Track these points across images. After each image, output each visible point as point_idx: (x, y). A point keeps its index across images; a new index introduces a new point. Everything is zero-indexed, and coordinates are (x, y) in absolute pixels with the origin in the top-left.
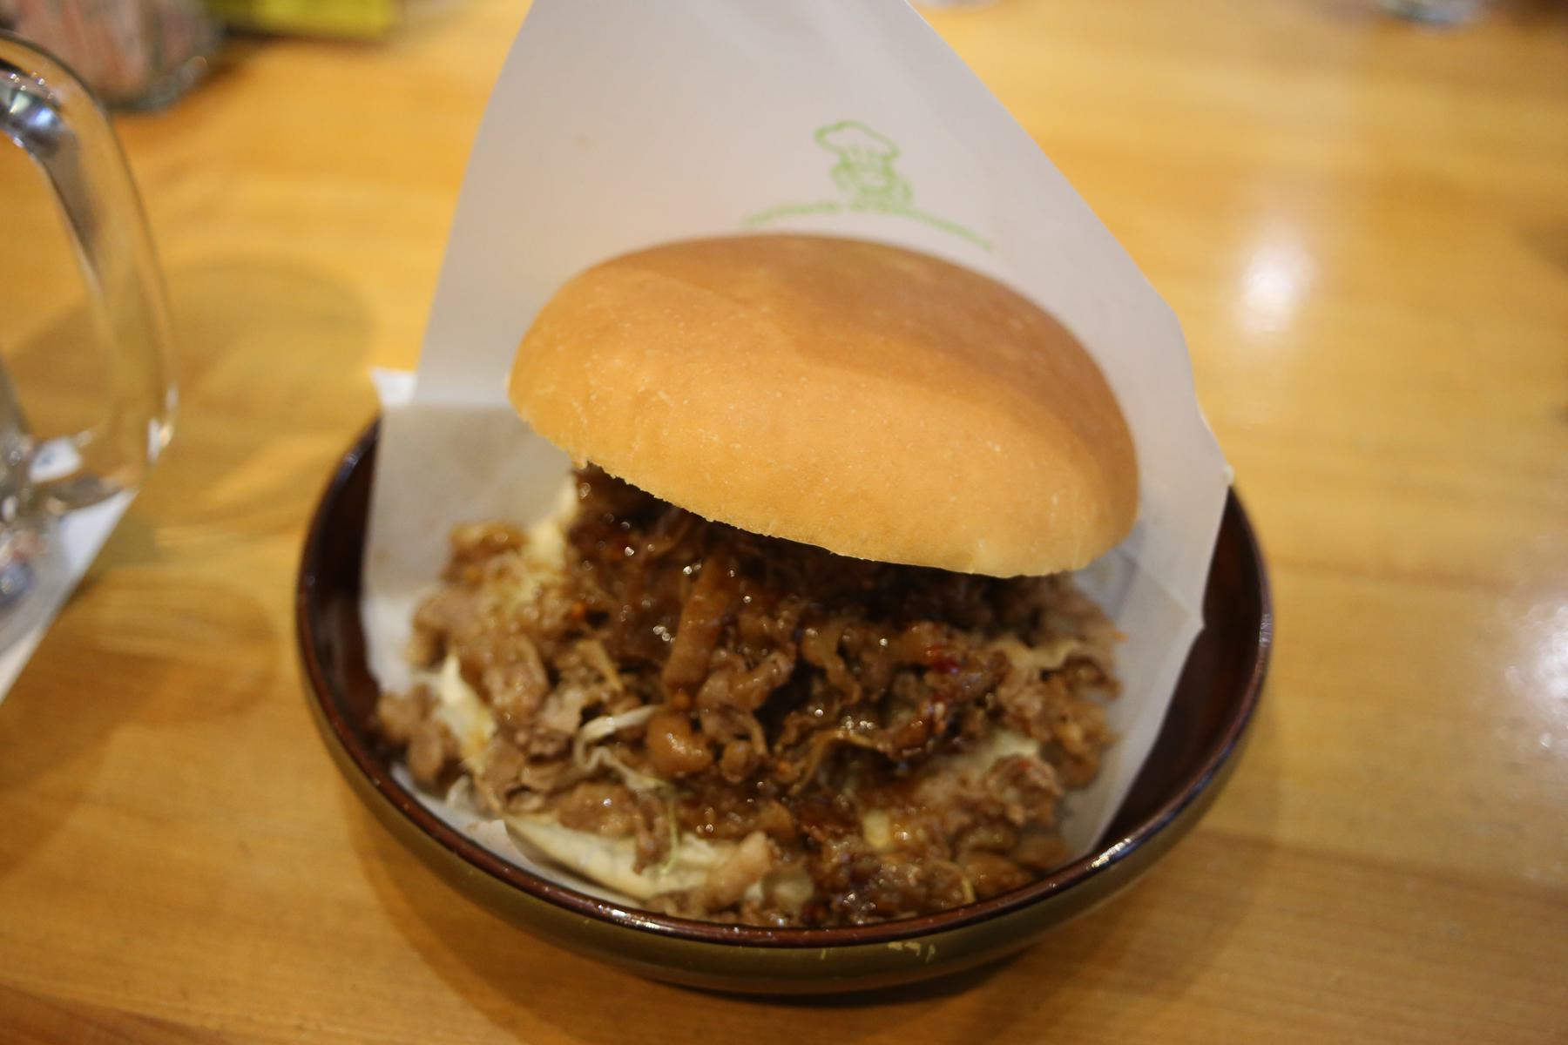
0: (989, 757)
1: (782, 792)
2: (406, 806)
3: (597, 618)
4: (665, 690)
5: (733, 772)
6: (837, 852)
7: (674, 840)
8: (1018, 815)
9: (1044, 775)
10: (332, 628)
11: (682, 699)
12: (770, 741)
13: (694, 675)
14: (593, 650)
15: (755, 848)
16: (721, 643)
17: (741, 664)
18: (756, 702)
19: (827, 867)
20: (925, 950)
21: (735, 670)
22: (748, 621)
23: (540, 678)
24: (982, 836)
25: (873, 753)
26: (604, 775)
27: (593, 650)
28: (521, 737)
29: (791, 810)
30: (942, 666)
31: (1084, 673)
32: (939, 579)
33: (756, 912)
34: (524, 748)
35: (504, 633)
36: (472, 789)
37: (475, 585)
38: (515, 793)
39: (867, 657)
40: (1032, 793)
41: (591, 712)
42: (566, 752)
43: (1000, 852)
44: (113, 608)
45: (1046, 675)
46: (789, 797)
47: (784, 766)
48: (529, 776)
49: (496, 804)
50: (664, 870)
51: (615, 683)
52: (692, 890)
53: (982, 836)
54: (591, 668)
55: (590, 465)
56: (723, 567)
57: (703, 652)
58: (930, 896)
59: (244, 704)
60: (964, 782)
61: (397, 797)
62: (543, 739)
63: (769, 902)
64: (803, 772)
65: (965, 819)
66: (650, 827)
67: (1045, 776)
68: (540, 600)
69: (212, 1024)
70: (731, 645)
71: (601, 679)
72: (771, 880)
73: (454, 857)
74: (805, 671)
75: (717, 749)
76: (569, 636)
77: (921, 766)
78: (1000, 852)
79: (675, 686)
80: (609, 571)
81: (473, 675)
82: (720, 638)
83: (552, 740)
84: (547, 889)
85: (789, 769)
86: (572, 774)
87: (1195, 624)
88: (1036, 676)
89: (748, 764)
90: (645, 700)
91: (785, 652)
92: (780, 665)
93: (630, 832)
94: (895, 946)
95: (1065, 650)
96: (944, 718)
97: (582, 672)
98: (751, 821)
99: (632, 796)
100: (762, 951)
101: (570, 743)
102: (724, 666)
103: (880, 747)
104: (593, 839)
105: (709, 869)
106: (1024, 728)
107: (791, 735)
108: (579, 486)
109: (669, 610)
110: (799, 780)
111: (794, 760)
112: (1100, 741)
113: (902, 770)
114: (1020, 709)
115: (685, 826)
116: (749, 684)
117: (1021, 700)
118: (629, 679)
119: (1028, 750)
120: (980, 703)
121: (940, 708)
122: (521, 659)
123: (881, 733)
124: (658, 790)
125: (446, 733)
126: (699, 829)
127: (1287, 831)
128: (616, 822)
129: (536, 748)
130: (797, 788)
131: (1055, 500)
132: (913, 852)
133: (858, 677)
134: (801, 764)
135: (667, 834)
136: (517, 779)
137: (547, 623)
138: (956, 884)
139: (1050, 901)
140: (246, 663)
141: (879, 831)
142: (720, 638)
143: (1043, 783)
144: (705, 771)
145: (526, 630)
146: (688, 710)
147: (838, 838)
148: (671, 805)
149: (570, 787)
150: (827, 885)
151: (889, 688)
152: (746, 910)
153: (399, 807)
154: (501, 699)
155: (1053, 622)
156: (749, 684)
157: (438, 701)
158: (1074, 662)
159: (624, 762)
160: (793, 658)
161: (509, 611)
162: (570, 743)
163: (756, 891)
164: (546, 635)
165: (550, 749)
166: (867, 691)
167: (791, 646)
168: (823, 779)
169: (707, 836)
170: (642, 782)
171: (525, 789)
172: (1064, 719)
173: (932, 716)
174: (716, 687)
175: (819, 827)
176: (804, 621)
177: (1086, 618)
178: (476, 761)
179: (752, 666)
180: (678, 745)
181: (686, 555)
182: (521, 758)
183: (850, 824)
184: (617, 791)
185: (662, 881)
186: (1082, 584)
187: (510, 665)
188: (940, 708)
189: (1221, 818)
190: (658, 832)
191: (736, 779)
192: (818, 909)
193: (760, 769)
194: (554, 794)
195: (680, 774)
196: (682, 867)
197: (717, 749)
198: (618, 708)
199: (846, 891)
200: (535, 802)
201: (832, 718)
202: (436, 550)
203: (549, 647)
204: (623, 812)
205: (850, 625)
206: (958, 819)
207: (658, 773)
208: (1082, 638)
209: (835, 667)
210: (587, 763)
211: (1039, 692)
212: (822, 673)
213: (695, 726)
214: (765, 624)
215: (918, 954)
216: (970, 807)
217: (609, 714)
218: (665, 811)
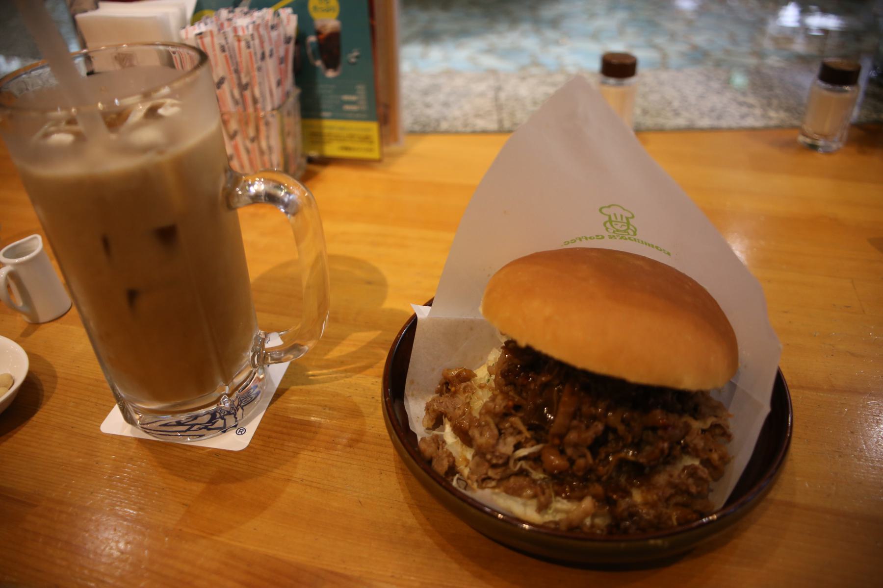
0: (680, 466)
1: (599, 480)
2: (444, 484)
3: (517, 408)
6: (623, 504)
7: (553, 499)
8: (693, 489)
9: (704, 472)
11: (557, 441)
14: (516, 420)
15: (587, 503)
17: (583, 426)
18: (589, 441)
19: (620, 510)
22: (585, 409)
23: (496, 432)
24: (679, 499)
26: (522, 473)
27: (516, 420)
30: (665, 427)
31: (718, 431)
40: (700, 480)
41: (518, 446)
42: (506, 464)
43: (684, 505)
44: (293, 402)
45: (704, 431)
48: (491, 473)
50: (550, 512)
51: (527, 434)
52: (561, 520)
53: (679, 499)
54: (515, 429)
60: (671, 476)
62: (497, 457)
65: (672, 491)
71: (520, 433)
73: (465, 505)
74: (609, 429)
75: (572, 462)
76: (505, 415)
77: (655, 470)
78: (684, 505)
80: (520, 389)
82: (574, 416)
83: (501, 458)
85: (602, 470)
86: (508, 472)
88: (700, 432)
90: (538, 442)
92: (600, 427)
93: (535, 496)
95: (710, 421)
97: (511, 430)
98: (586, 491)
99: (534, 481)
101: (508, 458)
104: (519, 499)
105: (567, 512)
106: (696, 453)
107: (603, 455)
112: (725, 460)
113: (647, 470)
115: (558, 494)
117: (696, 441)
118: (532, 433)
119: (697, 463)
120: (679, 443)
121: (666, 445)
124: (544, 478)
125: (450, 455)
126: (563, 495)
128: (529, 492)
129: (494, 461)
130: (605, 478)
132: (653, 505)
134: (606, 468)
135: (551, 497)
136: (486, 474)
138: (670, 518)
141: (637, 496)
143: (705, 476)
148: (551, 486)
149: (509, 477)
153: (440, 484)
157: (444, 442)
158: (715, 426)
159: (531, 467)
165: (501, 462)
168: (614, 474)
169: (568, 498)
170: (538, 475)
171: (489, 478)
172: (711, 450)
174: (572, 436)
176: (608, 409)
177: (717, 408)
179: (588, 427)
180: (555, 460)
183: (628, 494)
184: (528, 479)
185: (548, 517)
186: (713, 395)
189: (778, 494)
191: (580, 474)
192: (615, 528)
193: (590, 470)
194: (500, 481)
196: (557, 511)
197: (572, 462)
198: (528, 445)
199: (626, 520)
200: (493, 483)
202: (435, 379)
206: (669, 491)
208: (716, 416)
209: (621, 428)
212: (615, 431)
214: (593, 410)
217: (525, 447)
218: (549, 488)
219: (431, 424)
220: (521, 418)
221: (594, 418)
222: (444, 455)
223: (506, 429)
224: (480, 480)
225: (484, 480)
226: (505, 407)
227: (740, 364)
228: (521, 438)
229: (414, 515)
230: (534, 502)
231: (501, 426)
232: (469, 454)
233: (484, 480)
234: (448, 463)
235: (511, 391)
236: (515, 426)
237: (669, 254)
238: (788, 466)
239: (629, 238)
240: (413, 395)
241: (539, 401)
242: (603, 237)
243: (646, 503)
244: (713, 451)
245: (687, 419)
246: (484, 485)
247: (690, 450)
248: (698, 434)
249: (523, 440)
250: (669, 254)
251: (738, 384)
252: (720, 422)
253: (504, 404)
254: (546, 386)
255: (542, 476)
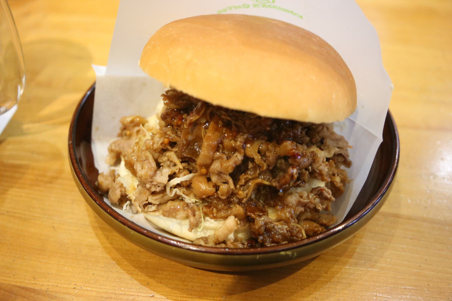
1: (240, 202)
3: (173, 144)
4: (198, 167)
5: (222, 195)
6: (260, 221)
10: (81, 153)
11: (204, 171)
12: (235, 184)
13: (208, 161)
14: (172, 155)
15: (231, 222)
16: (217, 150)
17: (225, 157)
18: (230, 171)
20: (293, 254)
21: (222, 159)
23: (154, 165)
25: (270, 187)
26: (177, 198)
27: (172, 155)
28: (148, 186)
29: (243, 208)
31: (340, 159)
32: (293, 124)
33: (232, 243)
34: (149, 189)
35: (139, 150)
36: (131, 205)
37: (130, 136)
38: (147, 204)
39: (268, 154)
41: (171, 177)
42: (164, 190)
45: (328, 159)
46: (242, 204)
47: (241, 192)
49: (140, 210)
50: (199, 230)
51: (180, 166)
53: (309, 215)
55: (171, 87)
56: (217, 123)
57: (211, 153)
58: (292, 236)
59: (53, 180)
61: (105, 208)
63: (236, 240)
64: (247, 194)
66: (194, 215)
67: (329, 194)
68: (152, 138)
69: (44, 288)
70: (221, 151)
71: (175, 165)
72: (236, 232)
73: (126, 227)
74: (247, 159)
75: (217, 188)
78: (312, 220)
79: (201, 166)
80: (176, 128)
81: (130, 166)
84: (160, 238)
85: (242, 193)
86: (166, 198)
87: (381, 140)
89: (228, 192)
90: (190, 172)
91: (240, 153)
92: (238, 157)
93: (187, 217)
94: (283, 253)
96: (296, 174)
97: (168, 163)
99: (187, 205)
100: (236, 257)
102: (218, 158)
103: (274, 184)
104: (174, 220)
105: (215, 229)
107: (243, 182)
108: (164, 100)
109: (199, 139)
110: (246, 197)
111: (244, 190)
114: (320, 171)
115: (206, 215)
116: (228, 164)
117: (321, 168)
120: (307, 169)
121: (295, 171)
122: (147, 159)
123: (274, 180)
124: (196, 202)
125: (122, 186)
127: (404, 211)
128: (182, 214)
129: (153, 189)
130: (245, 200)
131: (334, 96)
133: (265, 161)
134: (246, 192)
137: (155, 146)
138: (300, 231)
139: (333, 237)
140: (54, 166)
142: (217, 149)
144: (213, 195)
145: (148, 149)
146: (206, 174)
147: (260, 216)
149: (166, 202)
150: (257, 233)
151: (276, 164)
152: (229, 243)
154: (141, 172)
155: (328, 142)
156: (228, 164)
160: (243, 155)
161: (142, 143)
162: (165, 187)
163: (231, 236)
164: (155, 150)
165: (158, 190)
166: (268, 166)
167: (243, 151)
169: (215, 218)
170: (190, 200)
172: (334, 175)
173: (293, 173)
174: (216, 166)
175: (254, 213)
176: (246, 142)
178: (132, 195)
179: (228, 158)
181: (204, 121)
182: (148, 193)
184: (182, 203)
187: (143, 161)
188: (295, 171)
189: (384, 209)
190: (197, 216)
193: (233, 194)
195: (204, 197)
196: (206, 229)
197: (217, 188)
198: (181, 175)
200: (154, 208)
201: (257, 175)
203: (156, 155)
204: (184, 210)
205: (262, 143)
207: (195, 196)
209: (257, 158)
210: (170, 194)
211: (327, 165)
212: (253, 160)
213: (209, 180)
214: (233, 143)
215: (291, 256)
216: (305, 205)
219: (113, 161)
220: (176, 152)
221: (235, 150)
222: (117, 186)
223: (164, 162)
224: (141, 205)
225: (145, 206)
226: (162, 144)
227: (358, 104)
228: (175, 169)
229: (96, 235)
230: (187, 222)
231: (160, 161)
232: (136, 182)
233: (145, 206)
234: (120, 193)
235: (169, 131)
236: (170, 159)
237: (301, 17)
238: (395, 186)
239: (270, 6)
240: (99, 139)
241: (190, 138)
242: (248, 6)
243: (279, 220)
244: (336, 175)
245: (314, 149)
246: (146, 210)
247: (317, 175)
248: (323, 162)
249: (177, 171)
250: (301, 17)
251: (357, 122)
252: (342, 152)
253: (161, 141)
254: (195, 124)
255: (194, 200)
